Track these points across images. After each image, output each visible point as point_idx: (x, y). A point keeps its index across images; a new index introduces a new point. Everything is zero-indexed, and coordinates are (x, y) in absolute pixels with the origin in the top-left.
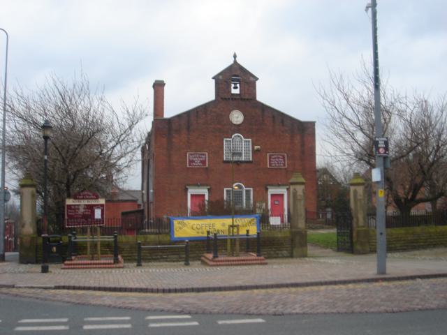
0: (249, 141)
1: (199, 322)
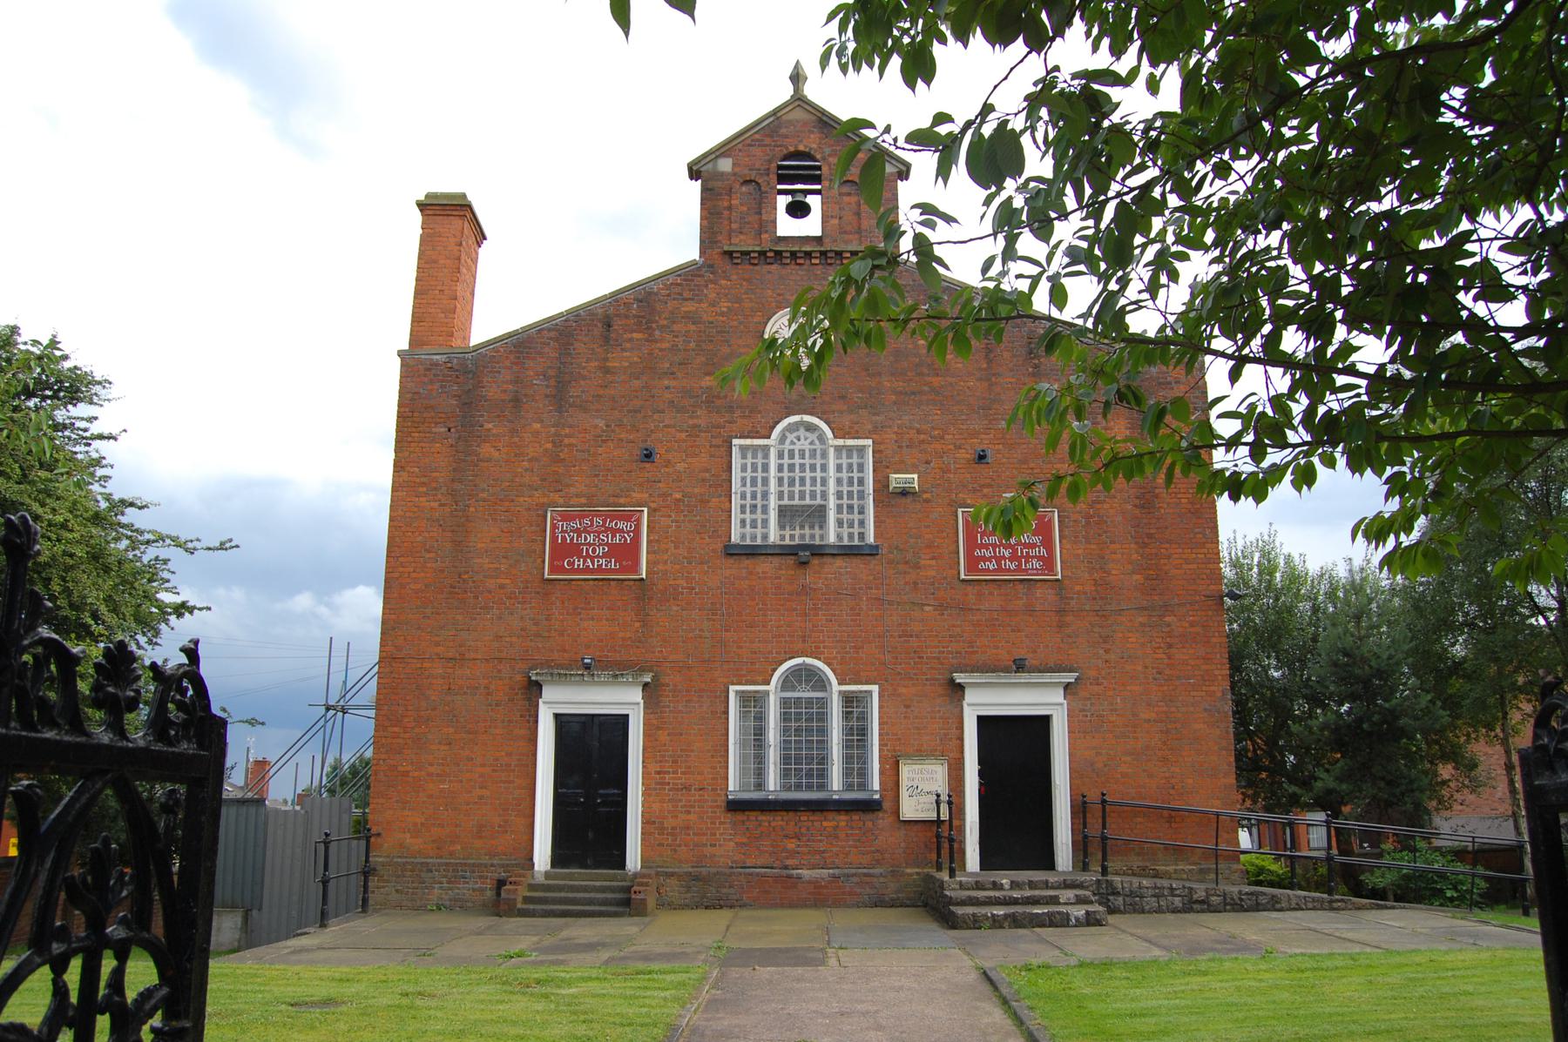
0: (861, 450)
1: (1481, 90)
